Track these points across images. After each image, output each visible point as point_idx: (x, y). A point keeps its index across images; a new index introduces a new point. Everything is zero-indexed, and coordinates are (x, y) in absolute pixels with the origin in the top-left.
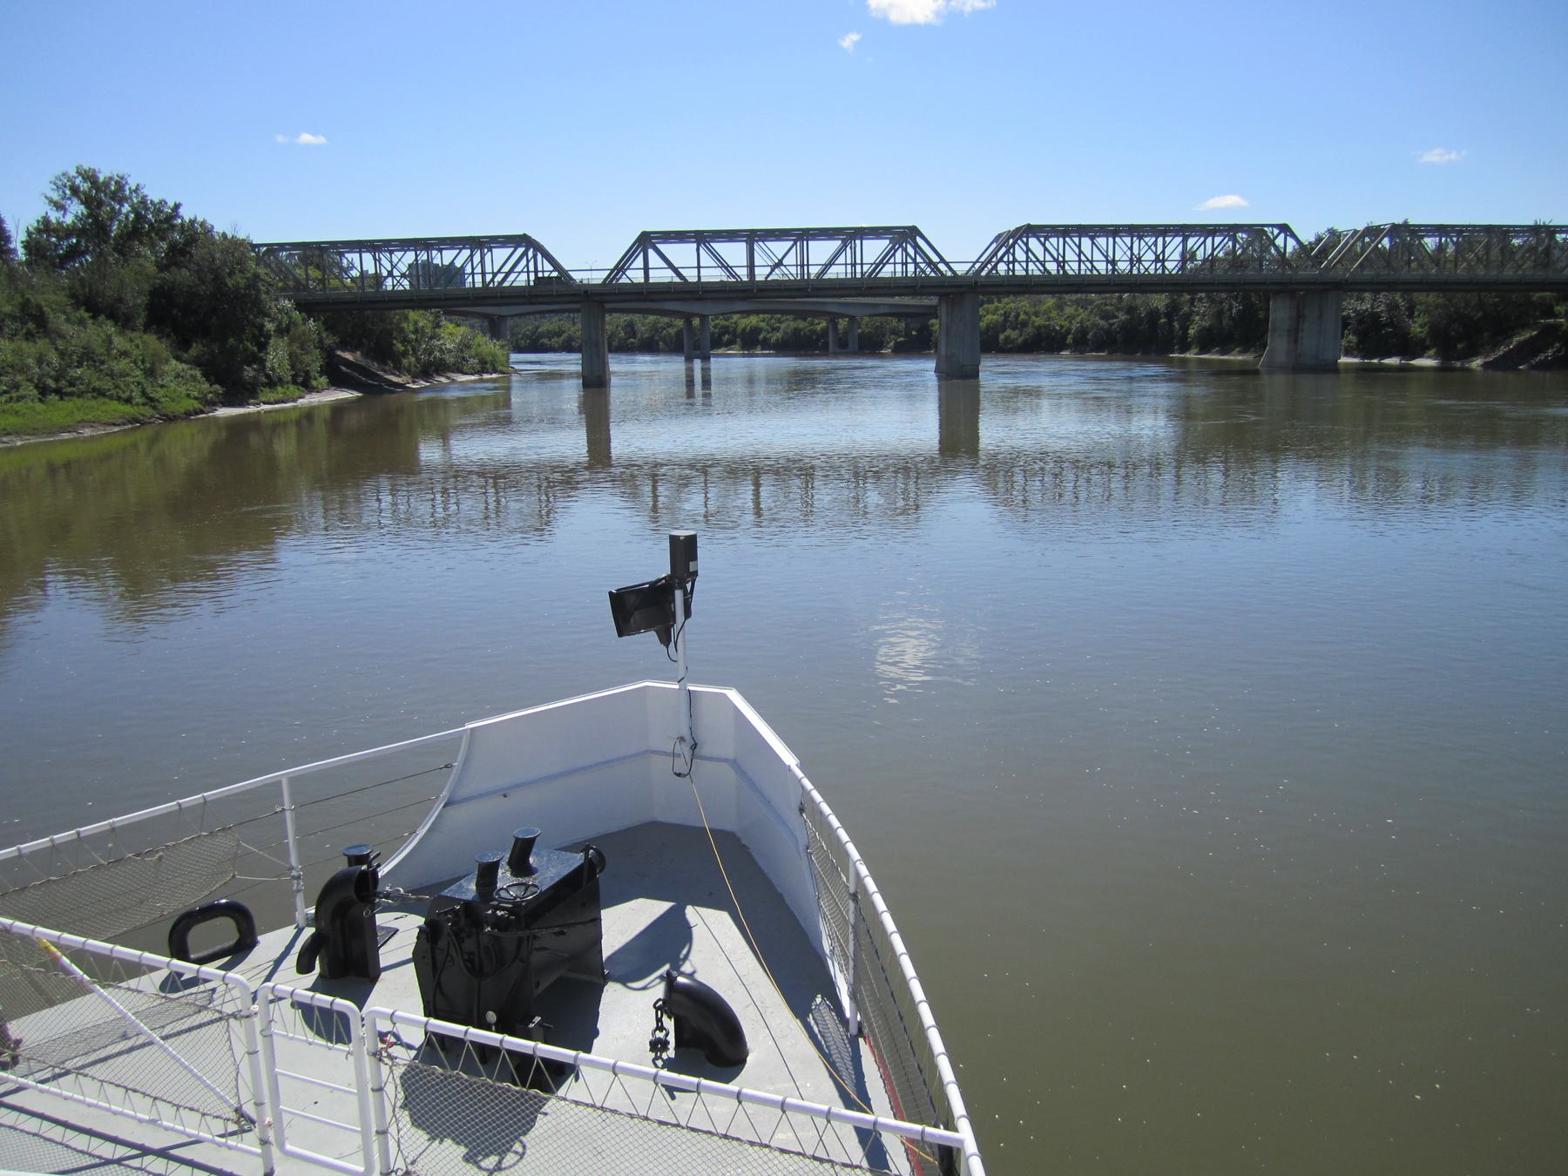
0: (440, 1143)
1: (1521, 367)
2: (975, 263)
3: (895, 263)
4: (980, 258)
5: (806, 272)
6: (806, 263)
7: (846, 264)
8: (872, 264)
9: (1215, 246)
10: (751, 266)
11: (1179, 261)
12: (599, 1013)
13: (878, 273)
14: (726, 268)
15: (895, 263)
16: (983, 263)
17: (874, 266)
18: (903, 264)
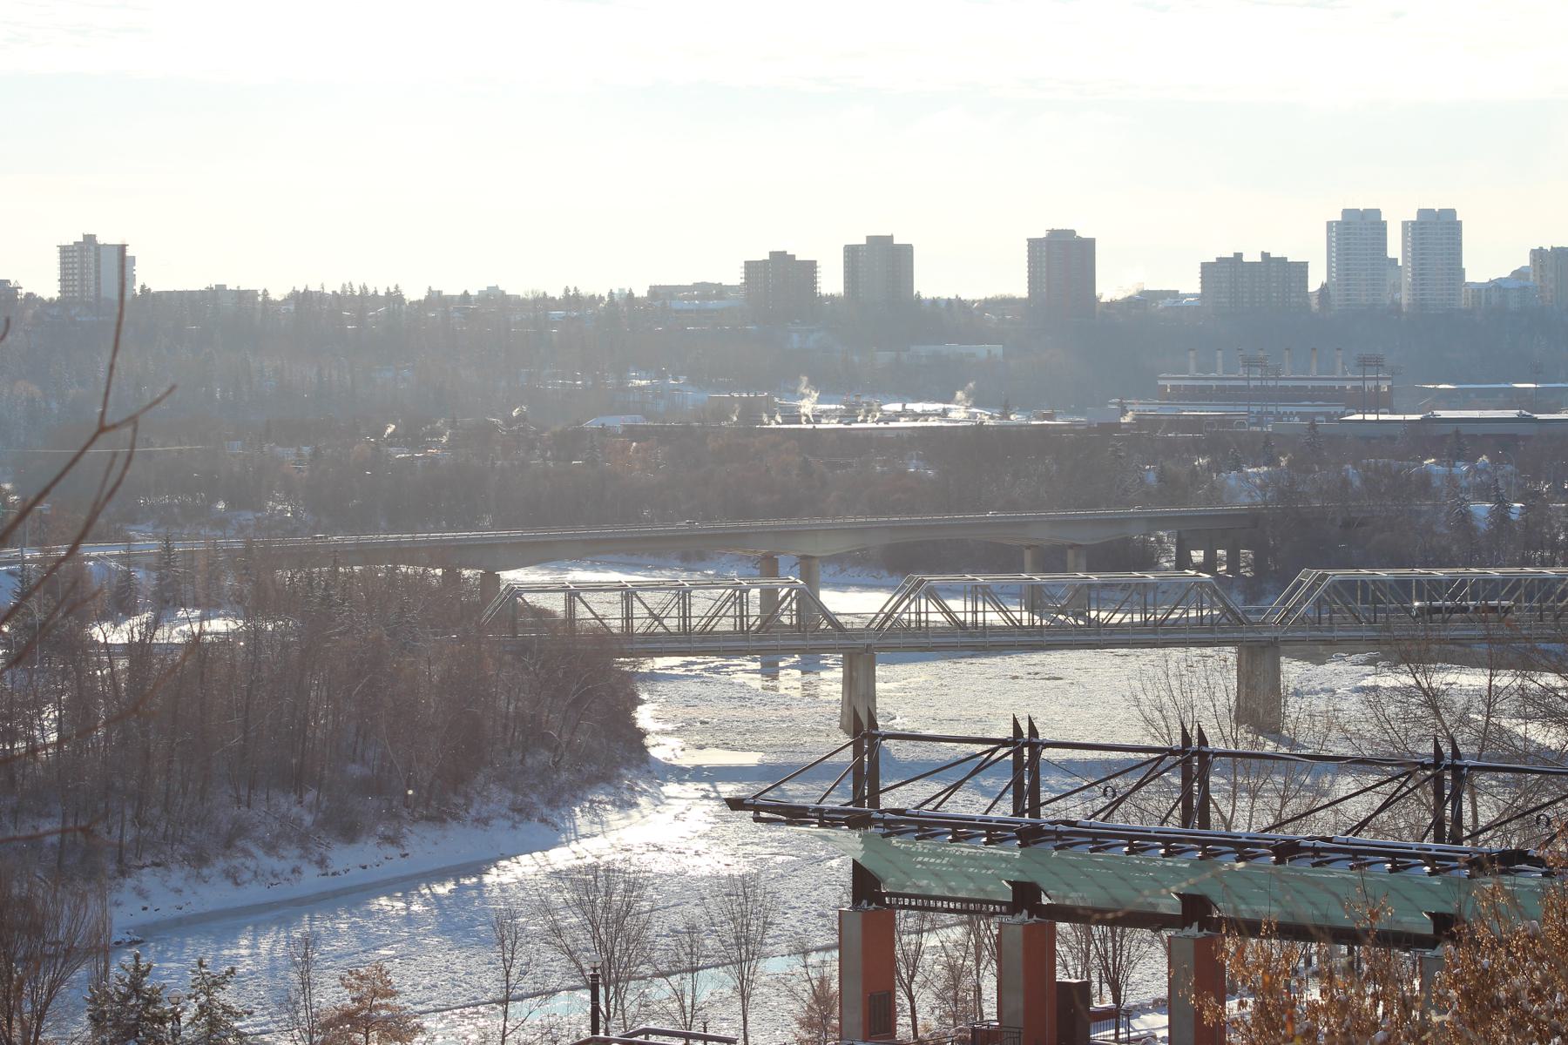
0: (823, 981)
1: (466, 573)
2: (877, 615)
3: (910, 613)
4: (719, 620)
5: (687, 602)
6: (688, 615)
7: (965, 612)
8: (724, 615)
9: (1013, 613)
10: (628, 617)
11: (759, 617)
12: (702, 283)
13: (1110, 619)
14: (948, 614)
15: (910, 613)
16: (886, 614)
17: (706, 619)
18: (973, 612)
